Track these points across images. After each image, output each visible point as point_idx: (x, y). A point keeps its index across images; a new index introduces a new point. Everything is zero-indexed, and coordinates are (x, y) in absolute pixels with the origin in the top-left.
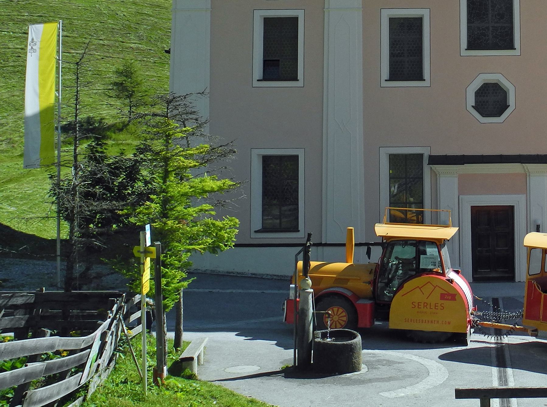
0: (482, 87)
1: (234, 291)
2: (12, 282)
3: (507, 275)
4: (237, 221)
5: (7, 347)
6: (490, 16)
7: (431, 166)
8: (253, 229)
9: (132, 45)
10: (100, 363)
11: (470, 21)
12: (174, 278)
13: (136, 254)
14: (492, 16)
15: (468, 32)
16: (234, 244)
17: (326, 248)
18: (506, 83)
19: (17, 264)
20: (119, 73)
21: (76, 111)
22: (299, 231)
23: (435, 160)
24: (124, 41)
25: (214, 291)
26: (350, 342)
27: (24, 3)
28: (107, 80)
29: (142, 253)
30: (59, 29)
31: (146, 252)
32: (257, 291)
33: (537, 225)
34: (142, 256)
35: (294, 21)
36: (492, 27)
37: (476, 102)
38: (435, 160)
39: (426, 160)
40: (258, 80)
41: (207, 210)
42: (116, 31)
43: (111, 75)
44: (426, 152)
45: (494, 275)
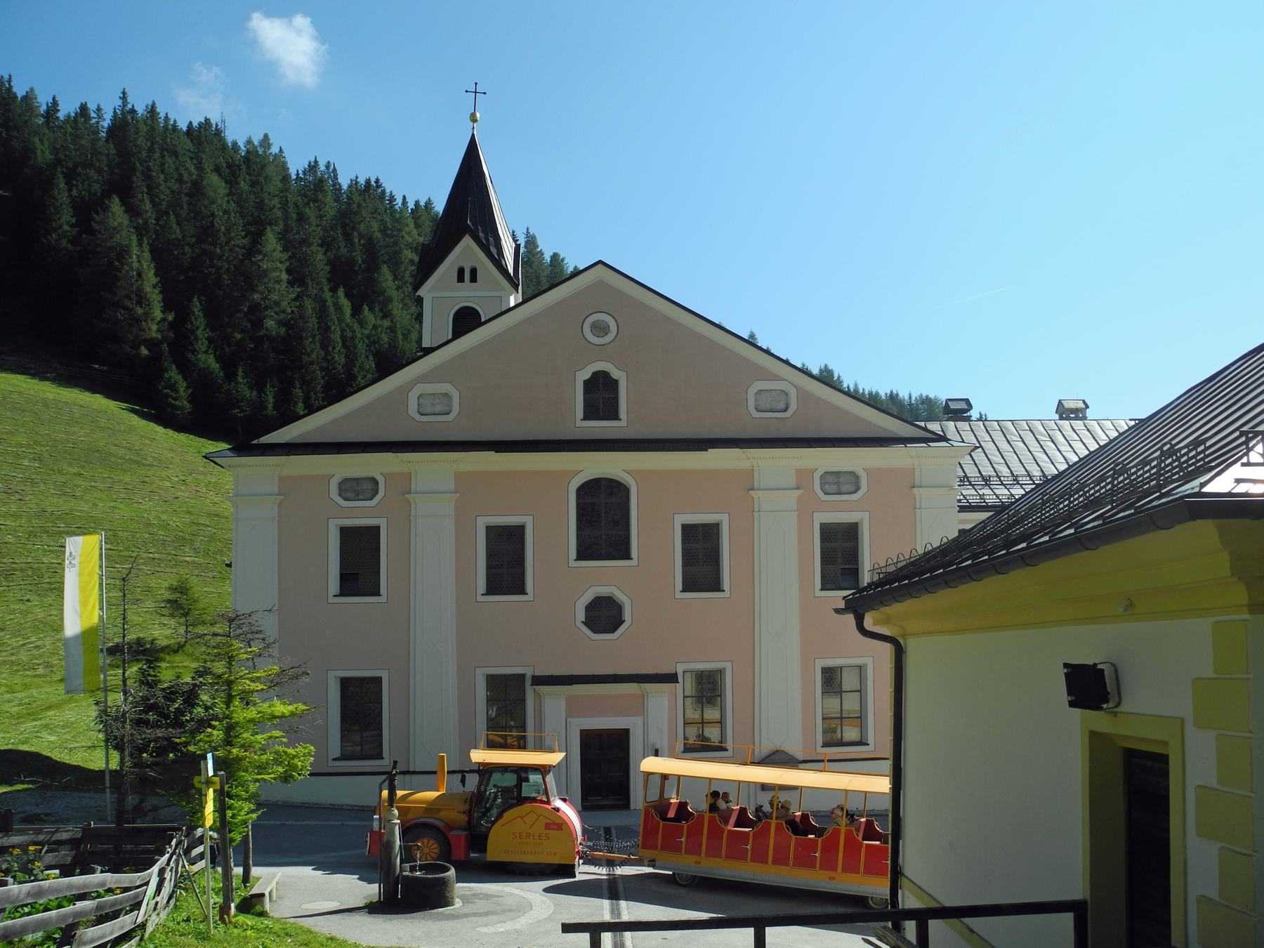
0: (593, 601)
1: (310, 823)
4: (312, 748)
8: (331, 757)
9: (187, 559)
11: (579, 528)
12: (240, 810)
13: (197, 785)
16: (309, 773)
18: (620, 596)
20: (172, 589)
23: (539, 681)
25: (287, 823)
27: (59, 513)
28: (159, 597)
30: (102, 542)
33: (656, 750)
34: (203, 786)
35: (377, 529)
39: (528, 681)
43: (163, 592)
44: (529, 673)
45: (606, 802)
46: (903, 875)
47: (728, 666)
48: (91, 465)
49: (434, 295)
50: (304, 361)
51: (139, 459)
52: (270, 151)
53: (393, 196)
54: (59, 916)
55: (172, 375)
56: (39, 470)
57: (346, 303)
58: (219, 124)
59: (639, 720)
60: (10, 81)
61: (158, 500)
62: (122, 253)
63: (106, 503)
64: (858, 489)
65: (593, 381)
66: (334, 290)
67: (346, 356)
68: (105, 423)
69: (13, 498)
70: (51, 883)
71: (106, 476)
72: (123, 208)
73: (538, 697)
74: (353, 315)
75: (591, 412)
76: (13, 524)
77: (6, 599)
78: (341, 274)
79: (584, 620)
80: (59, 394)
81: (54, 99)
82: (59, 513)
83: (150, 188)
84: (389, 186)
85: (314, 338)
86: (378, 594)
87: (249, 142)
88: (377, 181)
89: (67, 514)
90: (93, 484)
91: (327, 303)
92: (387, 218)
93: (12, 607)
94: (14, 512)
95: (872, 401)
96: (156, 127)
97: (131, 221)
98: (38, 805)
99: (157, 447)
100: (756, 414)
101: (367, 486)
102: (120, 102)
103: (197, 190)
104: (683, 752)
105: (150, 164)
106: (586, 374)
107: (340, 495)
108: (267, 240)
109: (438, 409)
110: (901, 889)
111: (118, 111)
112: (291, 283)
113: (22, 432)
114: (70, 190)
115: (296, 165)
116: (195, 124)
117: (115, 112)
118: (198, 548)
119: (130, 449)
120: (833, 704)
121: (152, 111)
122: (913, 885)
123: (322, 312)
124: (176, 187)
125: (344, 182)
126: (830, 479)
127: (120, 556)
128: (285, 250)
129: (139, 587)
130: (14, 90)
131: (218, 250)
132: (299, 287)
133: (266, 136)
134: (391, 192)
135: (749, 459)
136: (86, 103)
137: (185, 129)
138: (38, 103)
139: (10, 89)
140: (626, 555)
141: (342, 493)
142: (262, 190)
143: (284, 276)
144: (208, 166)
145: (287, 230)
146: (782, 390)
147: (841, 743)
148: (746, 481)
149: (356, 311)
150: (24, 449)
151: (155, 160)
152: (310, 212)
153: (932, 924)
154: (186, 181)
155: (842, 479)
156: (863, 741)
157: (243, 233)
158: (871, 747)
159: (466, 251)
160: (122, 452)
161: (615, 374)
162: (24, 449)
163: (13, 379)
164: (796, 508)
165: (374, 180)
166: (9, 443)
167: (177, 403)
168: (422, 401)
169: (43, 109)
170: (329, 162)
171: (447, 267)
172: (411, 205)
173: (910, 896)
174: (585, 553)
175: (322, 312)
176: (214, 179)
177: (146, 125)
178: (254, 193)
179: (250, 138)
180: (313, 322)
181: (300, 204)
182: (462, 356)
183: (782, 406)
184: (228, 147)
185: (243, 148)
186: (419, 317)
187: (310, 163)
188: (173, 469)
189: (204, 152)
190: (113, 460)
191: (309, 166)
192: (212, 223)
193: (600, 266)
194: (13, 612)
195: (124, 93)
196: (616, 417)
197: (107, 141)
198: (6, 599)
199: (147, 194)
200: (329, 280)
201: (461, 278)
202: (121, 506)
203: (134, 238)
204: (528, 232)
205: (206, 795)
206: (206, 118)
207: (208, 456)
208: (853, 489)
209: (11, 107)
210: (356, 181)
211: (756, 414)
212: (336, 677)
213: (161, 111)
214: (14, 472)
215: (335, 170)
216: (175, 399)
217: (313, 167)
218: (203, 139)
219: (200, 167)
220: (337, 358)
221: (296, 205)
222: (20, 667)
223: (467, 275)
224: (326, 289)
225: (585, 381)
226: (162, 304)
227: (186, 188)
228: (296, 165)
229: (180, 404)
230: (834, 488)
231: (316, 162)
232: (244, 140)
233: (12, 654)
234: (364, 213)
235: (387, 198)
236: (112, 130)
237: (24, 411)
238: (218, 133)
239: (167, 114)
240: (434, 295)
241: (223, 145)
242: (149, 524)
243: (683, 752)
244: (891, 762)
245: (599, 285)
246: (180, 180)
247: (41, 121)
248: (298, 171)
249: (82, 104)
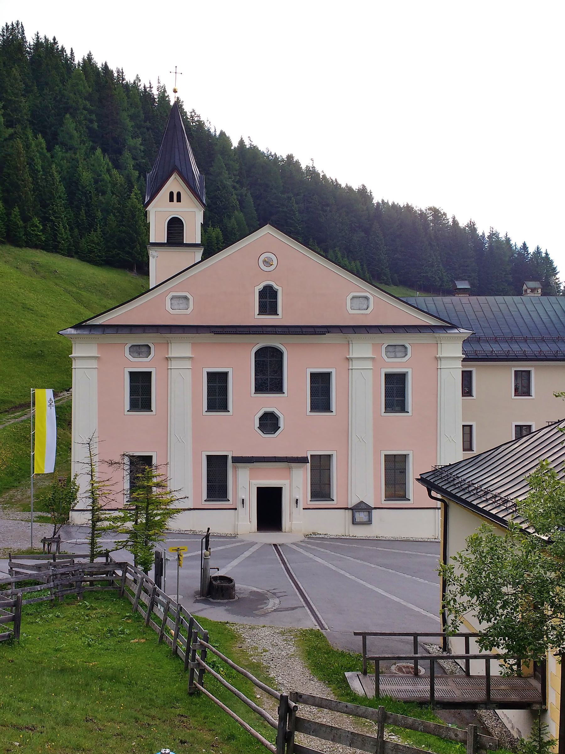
18: (277, 412)
23: (237, 460)
39: (230, 460)
47: (309, 413)
59: (287, 482)
79: (258, 426)
153: (492, 661)
158: (335, 502)
171: (164, 193)
196: (276, 313)
201: (171, 200)
208: (403, 355)
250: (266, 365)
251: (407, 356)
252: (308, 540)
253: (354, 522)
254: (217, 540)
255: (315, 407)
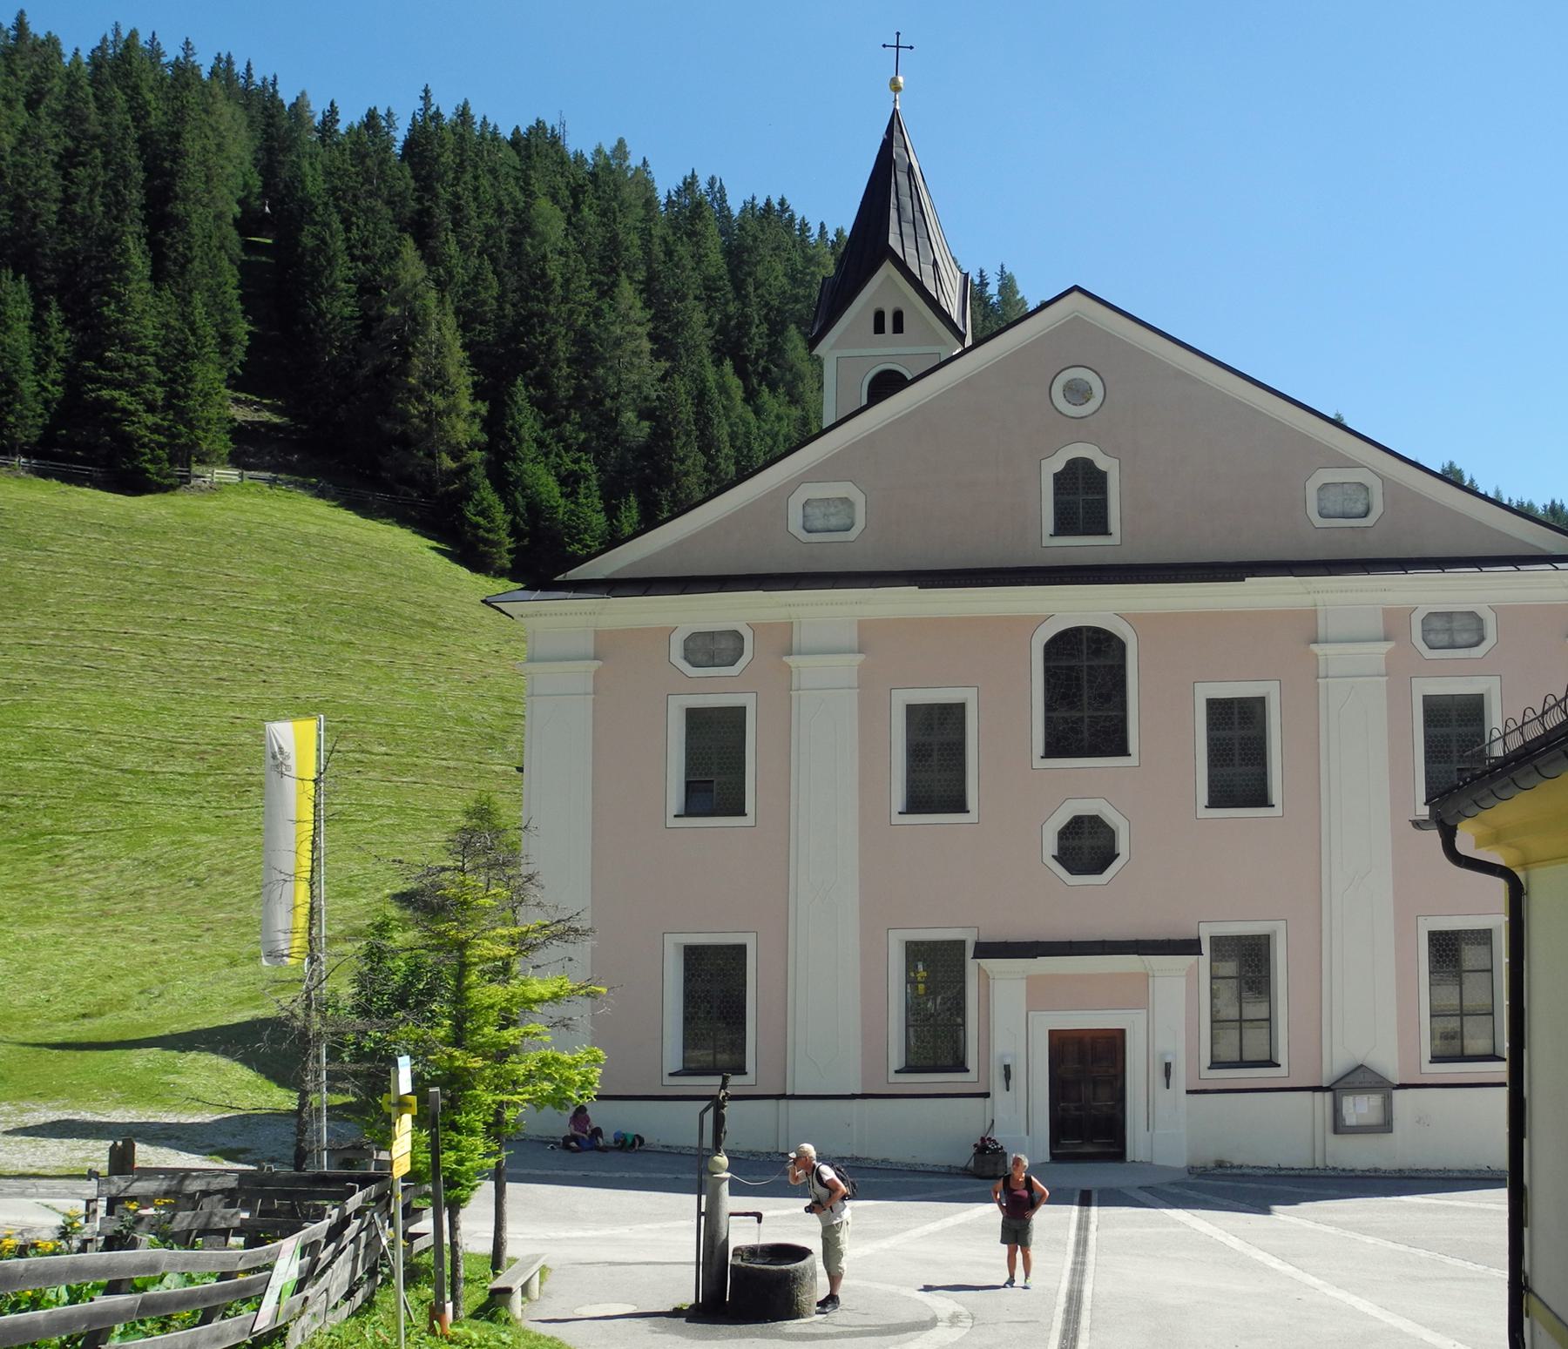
0: (1070, 823)
1: (627, 1175)
2: (255, 1154)
3: (1112, 1150)
4: (600, 1053)
5: (31, 1267)
6: (1085, 698)
7: (978, 960)
8: (667, 1070)
9: (497, 768)
10: (308, 1295)
11: (1049, 707)
12: (472, 1151)
13: (387, 1109)
14: (1089, 698)
15: (1046, 728)
16: (596, 1093)
17: (792, 1103)
18: (1112, 817)
19: (269, 1125)
20: (468, 814)
21: (313, 863)
22: (746, 1073)
23: (987, 950)
24: (482, 761)
25: (592, 1174)
26: (793, 1265)
27: (316, 700)
28: (452, 825)
29: (394, 1105)
30: (320, 730)
31: (402, 1104)
32: (669, 1176)
33: (1166, 1064)
34: (393, 1110)
35: (740, 712)
36: (1089, 717)
37: (1060, 848)
38: (987, 950)
39: (970, 952)
40: (675, 816)
41: (536, 1034)
42: (468, 743)
43: (459, 818)
44: (970, 938)
45: (1089, 1149)
46: (1530, 1291)
48: (365, 630)
49: (839, 353)
50: (675, 469)
51: (434, 620)
52: (627, 163)
53: (806, 225)
54: (53, 1320)
55: (484, 495)
56: (292, 637)
57: (735, 383)
58: (557, 128)
60: (274, 84)
61: (458, 681)
62: (415, 320)
63: (384, 684)
64: (1482, 639)
65: (1068, 474)
66: (718, 363)
67: (737, 463)
68: (388, 567)
69: (255, 678)
70: (30, 1264)
71: (386, 645)
72: (419, 253)
73: (985, 978)
74: (746, 400)
75: (1064, 525)
76: (253, 717)
77: (235, 828)
78: (729, 345)
79: (1056, 854)
80: (325, 526)
81: (332, 104)
82: (316, 700)
83: (457, 224)
84: (799, 210)
85: (688, 434)
86: (741, 812)
87: (599, 151)
88: (782, 202)
89: (327, 701)
90: (367, 657)
91: (708, 384)
92: (797, 257)
93: (244, 839)
94: (254, 699)
95: (1524, 512)
96: (467, 136)
97: (429, 271)
98: (234, 1136)
99: (461, 601)
100: (1320, 522)
101: (725, 644)
102: (421, 104)
103: (524, 227)
104: (1209, 1068)
105: (459, 189)
106: (1057, 464)
107: (686, 658)
108: (621, 292)
109: (834, 522)
110: (1527, 1316)
111: (418, 117)
112: (657, 355)
113: (271, 583)
114: (348, 230)
115: (665, 184)
116: (523, 130)
117: (414, 117)
118: (512, 752)
119: (421, 605)
120: (1449, 996)
121: (464, 114)
122: (1546, 1310)
123: (701, 397)
124: (494, 222)
125: (735, 206)
126: (1437, 624)
127: (400, 764)
128: (647, 305)
129: (424, 810)
130: (280, 96)
131: (552, 310)
132: (667, 360)
133: (621, 142)
134: (803, 218)
135: (1309, 593)
136: (375, 108)
137: (509, 137)
138: (311, 112)
139: (274, 95)
140: (1122, 750)
141: (691, 657)
142: (615, 220)
143: (647, 345)
144: (538, 187)
145: (652, 277)
146: (1361, 484)
147: (1463, 1058)
148: (1306, 627)
149: (750, 396)
150: (273, 607)
151: (465, 183)
152: (683, 250)
154: (508, 211)
155: (1456, 625)
156: (1497, 1054)
157: (588, 283)
159: (882, 288)
160: (408, 610)
161: (1102, 463)
162: (273, 607)
163: (264, 506)
164: (1383, 670)
165: (778, 201)
166: (254, 599)
167: (491, 536)
168: (809, 510)
169: (319, 118)
170: (713, 178)
172: (831, 236)
173: (1543, 1331)
174: (1058, 745)
175: (701, 397)
176: (544, 204)
177: (455, 134)
178: (604, 225)
179: (600, 146)
180: (687, 411)
181: (670, 239)
182: (870, 440)
183: (1360, 508)
184: (569, 159)
185: (590, 161)
186: (821, 388)
187: (685, 179)
188: (483, 634)
189: (534, 168)
190: (396, 621)
191: (684, 184)
192: (543, 270)
193: (1076, 295)
194: (245, 846)
195: (426, 91)
196: (1105, 531)
197: (403, 158)
198: (235, 828)
199: (452, 231)
200: (714, 350)
201: (879, 328)
202: (405, 689)
203: (433, 294)
204: (1002, 271)
205: (395, 1124)
206: (538, 120)
207: (489, 600)
208: (1475, 639)
209: (276, 119)
210: (752, 203)
211: (1320, 522)
212: (676, 945)
213: (477, 114)
214: (258, 641)
215: (722, 188)
216: (489, 531)
217: (690, 184)
218: (533, 150)
219: (529, 193)
220: (723, 466)
221: (664, 239)
222: (248, 929)
223: (888, 322)
224: (707, 362)
225: (1055, 475)
226: (471, 391)
227: (509, 222)
228: (665, 184)
229: (496, 538)
230: (1443, 638)
231: (693, 176)
232: (592, 148)
233: (240, 910)
234: (765, 251)
235: (797, 227)
236: (409, 144)
237: (276, 551)
238: (555, 141)
239: (485, 118)
240: (839, 353)
241: (562, 158)
242: (442, 716)
243: (1209, 1068)
244: (1508, 1089)
245: (1076, 323)
246: (500, 212)
247: (314, 137)
248: (669, 192)
249: (370, 110)
250: (1078, 679)
251: (1484, 643)
252: (1197, 1181)
253: (1339, 1127)
254: (921, 1180)
255: (1221, 797)
